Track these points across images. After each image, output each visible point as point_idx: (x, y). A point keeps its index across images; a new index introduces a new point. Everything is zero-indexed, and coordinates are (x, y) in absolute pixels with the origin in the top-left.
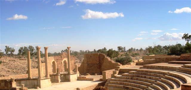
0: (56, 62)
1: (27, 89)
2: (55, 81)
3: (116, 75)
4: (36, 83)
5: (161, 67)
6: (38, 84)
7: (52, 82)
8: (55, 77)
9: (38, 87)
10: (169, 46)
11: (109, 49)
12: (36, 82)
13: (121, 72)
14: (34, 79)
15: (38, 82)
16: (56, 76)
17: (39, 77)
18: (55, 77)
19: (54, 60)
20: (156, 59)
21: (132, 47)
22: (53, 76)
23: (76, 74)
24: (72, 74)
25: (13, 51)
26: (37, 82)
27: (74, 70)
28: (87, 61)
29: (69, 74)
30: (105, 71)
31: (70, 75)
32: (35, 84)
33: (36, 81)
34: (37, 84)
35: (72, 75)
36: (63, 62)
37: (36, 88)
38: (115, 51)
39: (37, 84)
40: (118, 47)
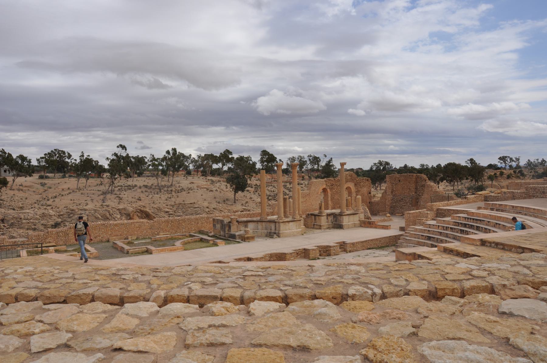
0: (328, 190)
2: (316, 227)
5: (415, 215)
8: (315, 219)
9: (275, 236)
12: (273, 226)
13: (440, 213)
15: (277, 226)
16: (317, 217)
18: (315, 219)
19: (325, 186)
20: (526, 190)
22: (313, 217)
25: (336, 168)
26: (275, 226)
31: (344, 217)
35: (347, 217)
38: (101, 166)
40: (543, 160)
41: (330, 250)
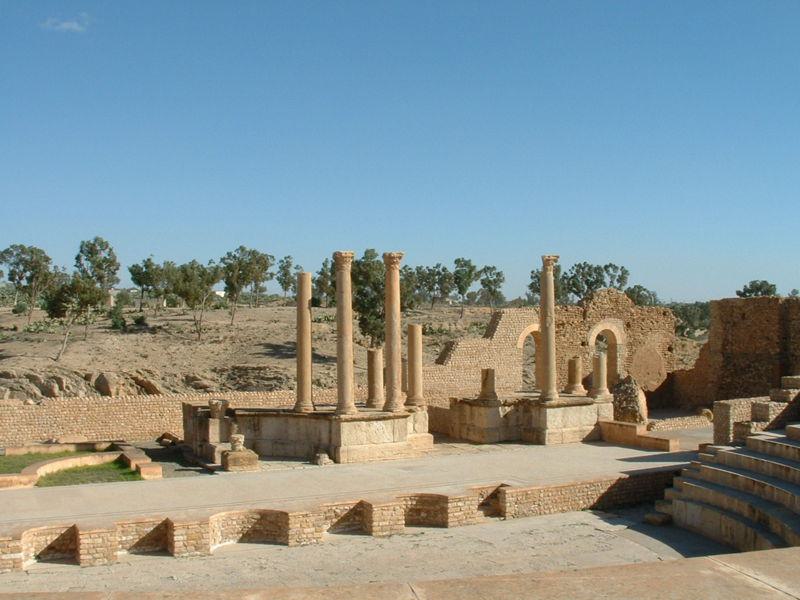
1: (250, 462)
3: (760, 433)
4: (325, 436)
6: (333, 442)
7: (437, 440)
9: (325, 458)
10: (61, 270)
11: (760, 277)
14: (316, 416)
17: (341, 405)
21: (630, 272)
22: (467, 407)
23: (591, 404)
24: (559, 406)
27: (587, 382)
28: (725, 340)
29: (542, 402)
30: (730, 402)
31: (548, 410)
32: (320, 440)
33: (327, 423)
34: (330, 440)
36: (592, 340)
37: (312, 460)
39: (330, 440)
41: (444, 511)
